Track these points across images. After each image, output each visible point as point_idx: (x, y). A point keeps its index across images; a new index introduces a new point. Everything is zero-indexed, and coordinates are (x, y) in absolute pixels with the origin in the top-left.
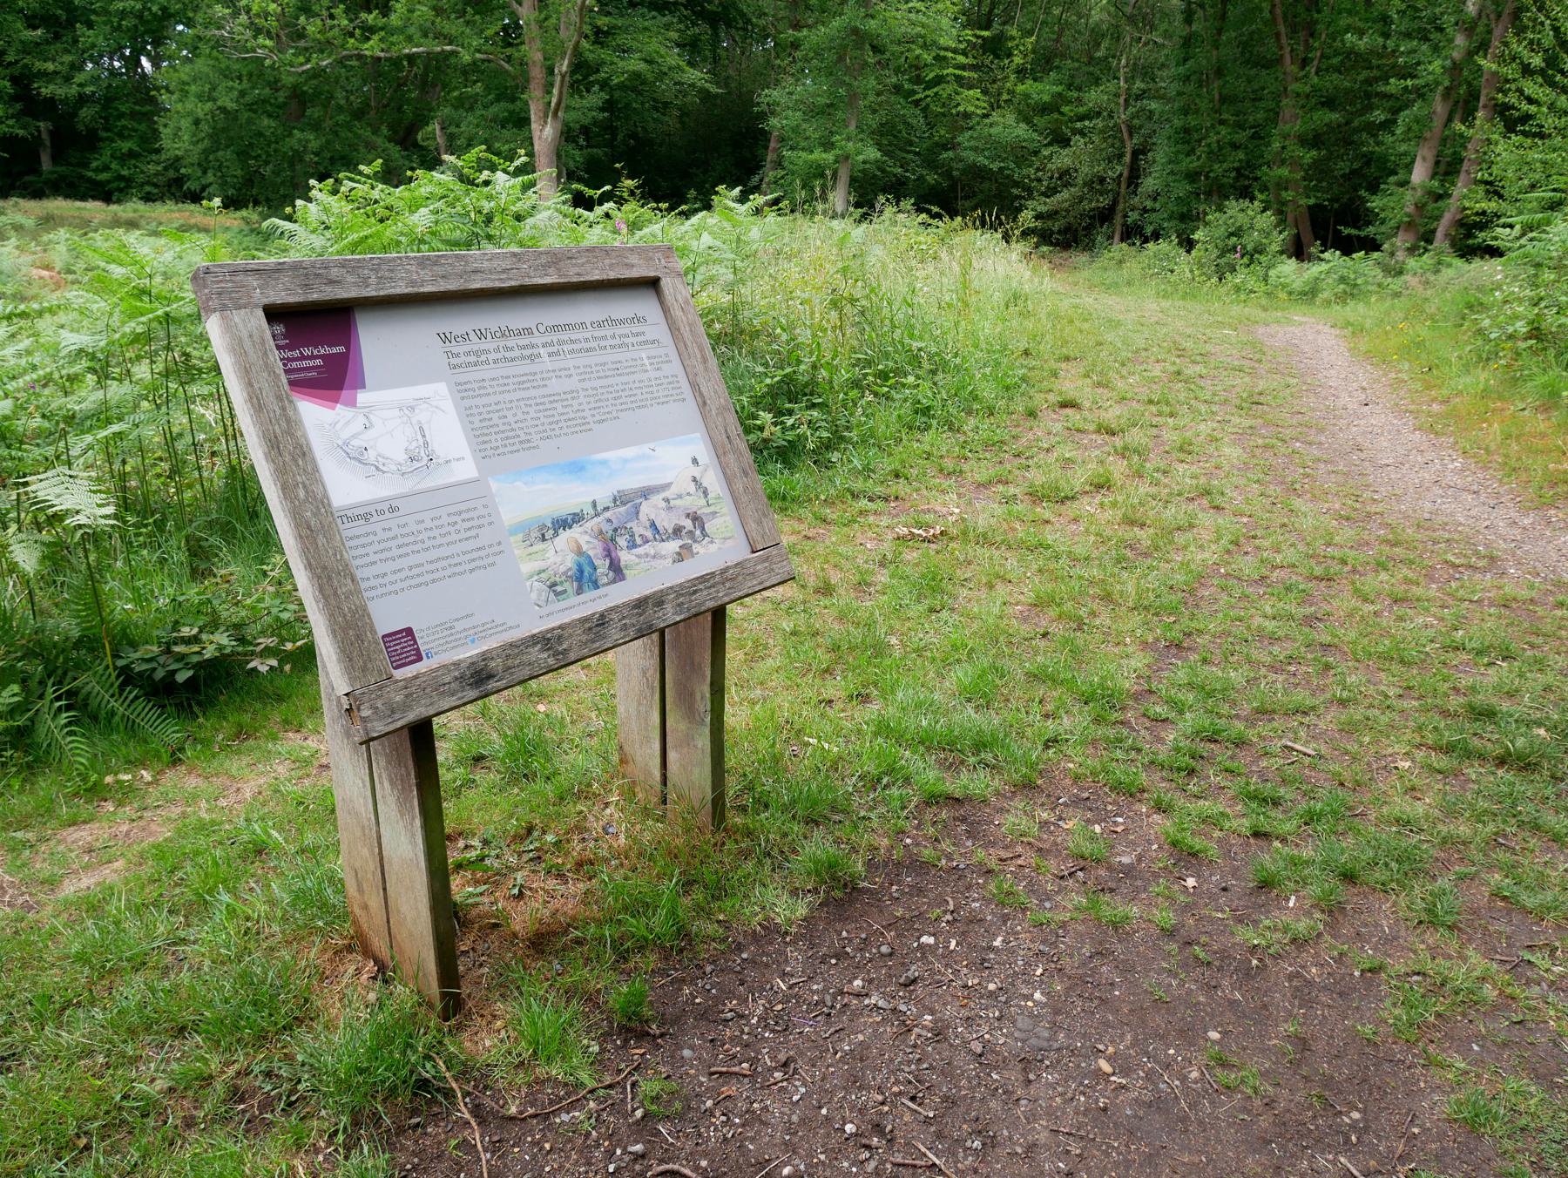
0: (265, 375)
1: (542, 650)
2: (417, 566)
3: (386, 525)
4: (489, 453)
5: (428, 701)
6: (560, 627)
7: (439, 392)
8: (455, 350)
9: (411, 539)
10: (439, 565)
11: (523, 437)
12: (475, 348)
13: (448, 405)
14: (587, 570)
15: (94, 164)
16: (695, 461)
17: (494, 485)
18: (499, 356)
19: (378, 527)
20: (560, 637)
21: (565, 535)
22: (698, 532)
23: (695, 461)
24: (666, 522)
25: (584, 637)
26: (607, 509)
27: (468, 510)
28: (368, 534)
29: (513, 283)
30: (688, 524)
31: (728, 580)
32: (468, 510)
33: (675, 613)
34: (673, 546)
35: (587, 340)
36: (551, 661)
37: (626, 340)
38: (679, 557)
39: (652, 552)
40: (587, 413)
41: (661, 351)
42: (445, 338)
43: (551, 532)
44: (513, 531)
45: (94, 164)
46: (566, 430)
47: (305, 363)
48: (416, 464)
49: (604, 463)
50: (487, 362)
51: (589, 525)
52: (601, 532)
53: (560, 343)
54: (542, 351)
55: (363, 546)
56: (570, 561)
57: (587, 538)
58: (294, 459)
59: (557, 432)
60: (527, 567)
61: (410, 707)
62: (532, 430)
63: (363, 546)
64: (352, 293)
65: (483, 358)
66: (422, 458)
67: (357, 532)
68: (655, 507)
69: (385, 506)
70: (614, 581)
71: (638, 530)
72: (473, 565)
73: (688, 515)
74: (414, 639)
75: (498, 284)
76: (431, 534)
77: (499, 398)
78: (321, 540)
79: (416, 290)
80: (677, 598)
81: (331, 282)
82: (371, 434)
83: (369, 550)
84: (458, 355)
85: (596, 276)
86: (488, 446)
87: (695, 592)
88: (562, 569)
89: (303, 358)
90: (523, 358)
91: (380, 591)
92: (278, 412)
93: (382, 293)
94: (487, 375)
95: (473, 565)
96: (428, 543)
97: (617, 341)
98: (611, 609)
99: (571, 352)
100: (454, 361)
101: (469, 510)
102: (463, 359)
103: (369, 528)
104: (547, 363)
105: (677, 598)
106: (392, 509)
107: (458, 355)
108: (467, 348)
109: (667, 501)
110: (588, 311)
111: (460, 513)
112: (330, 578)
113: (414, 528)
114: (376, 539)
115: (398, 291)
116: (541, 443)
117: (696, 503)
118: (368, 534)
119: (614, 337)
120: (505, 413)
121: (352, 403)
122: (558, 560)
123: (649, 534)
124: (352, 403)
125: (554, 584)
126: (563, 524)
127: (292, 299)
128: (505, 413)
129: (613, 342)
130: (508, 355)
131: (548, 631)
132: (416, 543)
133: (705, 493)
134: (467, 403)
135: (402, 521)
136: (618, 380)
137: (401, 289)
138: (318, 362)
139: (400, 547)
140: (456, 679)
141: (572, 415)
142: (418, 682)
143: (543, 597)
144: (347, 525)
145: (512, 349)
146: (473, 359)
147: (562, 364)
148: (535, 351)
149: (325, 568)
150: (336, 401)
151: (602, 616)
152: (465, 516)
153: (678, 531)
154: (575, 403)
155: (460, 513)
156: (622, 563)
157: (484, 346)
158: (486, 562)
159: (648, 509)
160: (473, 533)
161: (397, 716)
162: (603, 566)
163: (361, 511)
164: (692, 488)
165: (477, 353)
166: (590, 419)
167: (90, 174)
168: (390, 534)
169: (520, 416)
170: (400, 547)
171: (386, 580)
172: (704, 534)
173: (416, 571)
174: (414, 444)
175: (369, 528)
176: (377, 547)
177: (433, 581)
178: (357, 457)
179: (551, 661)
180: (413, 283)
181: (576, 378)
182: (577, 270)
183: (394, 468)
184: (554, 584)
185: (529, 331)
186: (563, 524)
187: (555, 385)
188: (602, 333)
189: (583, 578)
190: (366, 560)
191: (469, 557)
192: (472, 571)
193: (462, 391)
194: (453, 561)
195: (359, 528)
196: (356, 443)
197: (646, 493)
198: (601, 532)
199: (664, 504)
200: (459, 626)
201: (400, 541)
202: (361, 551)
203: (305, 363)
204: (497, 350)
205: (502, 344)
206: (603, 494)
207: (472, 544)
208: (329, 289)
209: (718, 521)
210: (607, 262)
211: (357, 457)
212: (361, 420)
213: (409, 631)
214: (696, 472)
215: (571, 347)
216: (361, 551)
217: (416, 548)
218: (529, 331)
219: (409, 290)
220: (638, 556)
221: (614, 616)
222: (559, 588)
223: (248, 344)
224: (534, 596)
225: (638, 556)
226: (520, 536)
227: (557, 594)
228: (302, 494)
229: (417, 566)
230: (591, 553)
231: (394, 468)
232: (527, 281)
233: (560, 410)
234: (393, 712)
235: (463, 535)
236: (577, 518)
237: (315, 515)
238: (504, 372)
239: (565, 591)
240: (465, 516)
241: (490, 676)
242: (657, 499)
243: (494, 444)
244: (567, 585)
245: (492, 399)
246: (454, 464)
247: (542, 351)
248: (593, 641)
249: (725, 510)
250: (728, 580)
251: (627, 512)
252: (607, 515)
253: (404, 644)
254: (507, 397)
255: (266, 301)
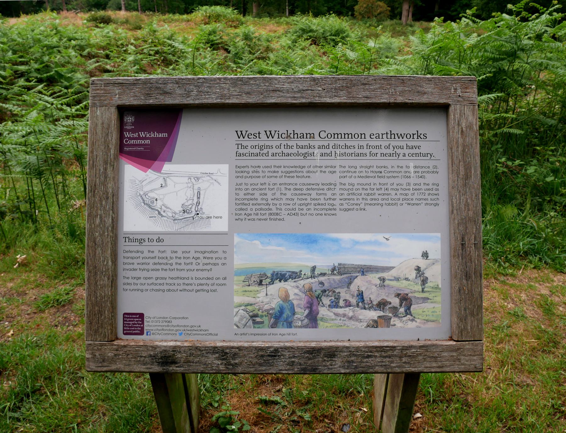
0: (103, 147)
1: (218, 359)
2: (162, 278)
3: (151, 249)
4: (243, 217)
5: (127, 363)
6: (238, 348)
7: (222, 171)
8: (244, 144)
9: (164, 261)
10: (176, 282)
11: (274, 211)
12: (261, 143)
13: (225, 181)
14: (287, 313)
15: (452, 9)
16: (425, 255)
17: (237, 239)
18: (279, 151)
19: (145, 249)
20: (235, 354)
21: (279, 285)
22: (402, 310)
23: (425, 255)
24: (374, 295)
25: (255, 361)
26: (323, 274)
27: (212, 252)
28: (138, 252)
29: (304, 101)
30: (396, 302)
31: (406, 355)
32: (212, 252)
33: (343, 367)
34: (374, 314)
35: (361, 147)
36: (222, 367)
37: (399, 151)
38: (375, 324)
39: (351, 314)
40: (337, 202)
41: (431, 164)
42: (240, 135)
43: (269, 280)
44: (239, 273)
45: (452, 9)
46: (312, 212)
47: (139, 142)
48: (186, 215)
49: (336, 241)
50: (267, 154)
51: (301, 283)
52: (310, 290)
53: (335, 147)
54: (316, 151)
55: (132, 258)
56: (275, 303)
57: (297, 291)
58: (101, 200)
59: (304, 212)
60: (238, 299)
61: (115, 362)
62: (283, 207)
63: (132, 258)
64: (177, 101)
65: (265, 151)
66: (193, 212)
67: (132, 249)
68: (369, 282)
69: (155, 238)
70: (306, 326)
71: (344, 295)
72: (200, 288)
73: (398, 295)
74: (143, 323)
75: (290, 101)
76: (179, 261)
77: (266, 180)
78: (99, 251)
79: (223, 101)
80: (350, 356)
81: (166, 93)
82: (163, 191)
83: (135, 261)
84: (246, 147)
85: (384, 99)
86: (243, 212)
87: (368, 357)
88: (266, 307)
89: (139, 138)
90: (298, 154)
91: (132, 287)
92: (102, 170)
93: (197, 102)
94: (263, 163)
95: (200, 288)
96: (174, 266)
97: (391, 151)
98: (286, 348)
99: (342, 155)
100: (241, 151)
101: (213, 252)
102: (249, 150)
103: (140, 248)
104: (318, 161)
105: (350, 356)
106: (159, 240)
107: (246, 147)
108: (256, 143)
109: (383, 280)
110: (380, 125)
111: (205, 252)
112: (96, 273)
113: (169, 254)
114: (142, 256)
115: (210, 101)
116: (286, 217)
117: (412, 288)
118: (138, 252)
119: (388, 147)
120: (267, 191)
121: (159, 170)
122: (266, 300)
123: (354, 301)
124: (159, 170)
125: (256, 316)
126: (281, 277)
127: (135, 103)
128: (267, 191)
129: (384, 151)
130: (286, 151)
131: (227, 348)
132: (167, 264)
133: (425, 282)
134: (239, 181)
135: (162, 249)
136: (377, 181)
137: (213, 99)
138: (147, 142)
139: (155, 264)
140: (151, 356)
141: (322, 201)
142: (125, 349)
143: (243, 322)
144: (127, 243)
145: (291, 147)
146: (257, 151)
147: (329, 163)
148: (311, 151)
149: (95, 267)
150: (149, 167)
151: (276, 350)
152: (207, 255)
153: (382, 305)
154: (329, 194)
155: (205, 252)
156: (320, 316)
157: (270, 143)
158: (210, 288)
159: (360, 283)
160: (208, 267)
161: (105, 364)
162: (301, 313)
163: (139, 237)
164: (413, 275)
165: (261, 148)
166: (338, 207)
167: (450, 13)
168: (152, 255)
169: (278, 195)
170: (155, 264)
171: (139, 281)
172: (408, 312)
173: (159, 281)
174: (190, 202)
175: (140, 248)
176: (140, 261)
177: (169, 290)
178: (148, 204)
179: (222, 367)
180: (222, 96)
181: (338, 174)
182: (368, 93)
183: (170, 215)
184: (256, 316)
185: (312, 136)
186: (281, 277)
187: (317, 178)
188: (378, 143)
189: (280, 317)
190: (131, 267)
191: (161, 287)
192: (197, 291)
193: (239, 172)
194: (186, 281)
195: (134, 247)
196: (152, 195)
197: (364, 270)
198: (310, 290)
199: (378, 282)
200: (175, 322)
201: (156, 261)
202: (130, 261)
203: (139, 142)
204: (279, 147)
205: (285, 143)
206: (324, 262)
207: (205, 274)
208: (162, 97)
209: (427, 306)
210: (400, 89)
211: (148, 204)
212: (161, 181)
213: (141, 316)
214: (422, 264)
215: (343, 151)
216: (130, 261)
217: (165, 267)
218: (312, 136)
219: (219, 101)
220: (336, 314)
221: (287, 354)
222: (258, 319)
223: (100, 127)
224: (236, 319)
225: (336, 314)
226: (243, 278)
227: (255, 322)
228: (98, 221)
229: (162, 278)
230: (295, 302)
231: (170, 215)
232: (317, 100)
233: (314, 196)
234: (104, 361)
235: (201, 267)
236: (295, 275)
237: (101, 235)
238: (278, 163)
239: (262, 323)
240: (207, 255)
241: (174, 362)
242: (374, 278)
243: (249, 212)
244: (266, 319)
245: (261, 180)
246: (212, 220)
247: (316, 151)
248: (261, 365)
249: (439, 299)
250: (406, 355)
251: (340, 281)
252: (322, 279)
253: (135, 322)
254: (273, 180)
255: (120, 103)
